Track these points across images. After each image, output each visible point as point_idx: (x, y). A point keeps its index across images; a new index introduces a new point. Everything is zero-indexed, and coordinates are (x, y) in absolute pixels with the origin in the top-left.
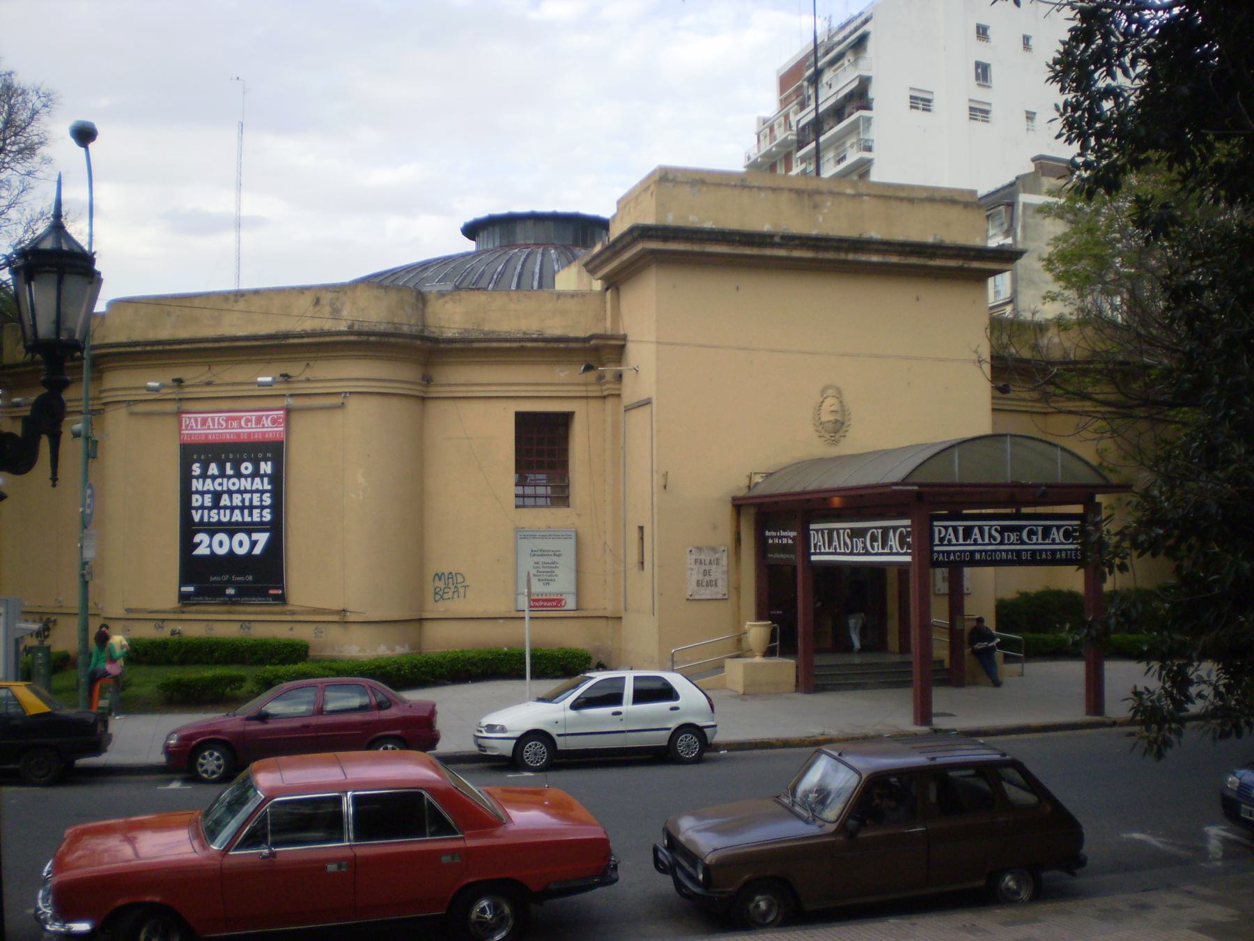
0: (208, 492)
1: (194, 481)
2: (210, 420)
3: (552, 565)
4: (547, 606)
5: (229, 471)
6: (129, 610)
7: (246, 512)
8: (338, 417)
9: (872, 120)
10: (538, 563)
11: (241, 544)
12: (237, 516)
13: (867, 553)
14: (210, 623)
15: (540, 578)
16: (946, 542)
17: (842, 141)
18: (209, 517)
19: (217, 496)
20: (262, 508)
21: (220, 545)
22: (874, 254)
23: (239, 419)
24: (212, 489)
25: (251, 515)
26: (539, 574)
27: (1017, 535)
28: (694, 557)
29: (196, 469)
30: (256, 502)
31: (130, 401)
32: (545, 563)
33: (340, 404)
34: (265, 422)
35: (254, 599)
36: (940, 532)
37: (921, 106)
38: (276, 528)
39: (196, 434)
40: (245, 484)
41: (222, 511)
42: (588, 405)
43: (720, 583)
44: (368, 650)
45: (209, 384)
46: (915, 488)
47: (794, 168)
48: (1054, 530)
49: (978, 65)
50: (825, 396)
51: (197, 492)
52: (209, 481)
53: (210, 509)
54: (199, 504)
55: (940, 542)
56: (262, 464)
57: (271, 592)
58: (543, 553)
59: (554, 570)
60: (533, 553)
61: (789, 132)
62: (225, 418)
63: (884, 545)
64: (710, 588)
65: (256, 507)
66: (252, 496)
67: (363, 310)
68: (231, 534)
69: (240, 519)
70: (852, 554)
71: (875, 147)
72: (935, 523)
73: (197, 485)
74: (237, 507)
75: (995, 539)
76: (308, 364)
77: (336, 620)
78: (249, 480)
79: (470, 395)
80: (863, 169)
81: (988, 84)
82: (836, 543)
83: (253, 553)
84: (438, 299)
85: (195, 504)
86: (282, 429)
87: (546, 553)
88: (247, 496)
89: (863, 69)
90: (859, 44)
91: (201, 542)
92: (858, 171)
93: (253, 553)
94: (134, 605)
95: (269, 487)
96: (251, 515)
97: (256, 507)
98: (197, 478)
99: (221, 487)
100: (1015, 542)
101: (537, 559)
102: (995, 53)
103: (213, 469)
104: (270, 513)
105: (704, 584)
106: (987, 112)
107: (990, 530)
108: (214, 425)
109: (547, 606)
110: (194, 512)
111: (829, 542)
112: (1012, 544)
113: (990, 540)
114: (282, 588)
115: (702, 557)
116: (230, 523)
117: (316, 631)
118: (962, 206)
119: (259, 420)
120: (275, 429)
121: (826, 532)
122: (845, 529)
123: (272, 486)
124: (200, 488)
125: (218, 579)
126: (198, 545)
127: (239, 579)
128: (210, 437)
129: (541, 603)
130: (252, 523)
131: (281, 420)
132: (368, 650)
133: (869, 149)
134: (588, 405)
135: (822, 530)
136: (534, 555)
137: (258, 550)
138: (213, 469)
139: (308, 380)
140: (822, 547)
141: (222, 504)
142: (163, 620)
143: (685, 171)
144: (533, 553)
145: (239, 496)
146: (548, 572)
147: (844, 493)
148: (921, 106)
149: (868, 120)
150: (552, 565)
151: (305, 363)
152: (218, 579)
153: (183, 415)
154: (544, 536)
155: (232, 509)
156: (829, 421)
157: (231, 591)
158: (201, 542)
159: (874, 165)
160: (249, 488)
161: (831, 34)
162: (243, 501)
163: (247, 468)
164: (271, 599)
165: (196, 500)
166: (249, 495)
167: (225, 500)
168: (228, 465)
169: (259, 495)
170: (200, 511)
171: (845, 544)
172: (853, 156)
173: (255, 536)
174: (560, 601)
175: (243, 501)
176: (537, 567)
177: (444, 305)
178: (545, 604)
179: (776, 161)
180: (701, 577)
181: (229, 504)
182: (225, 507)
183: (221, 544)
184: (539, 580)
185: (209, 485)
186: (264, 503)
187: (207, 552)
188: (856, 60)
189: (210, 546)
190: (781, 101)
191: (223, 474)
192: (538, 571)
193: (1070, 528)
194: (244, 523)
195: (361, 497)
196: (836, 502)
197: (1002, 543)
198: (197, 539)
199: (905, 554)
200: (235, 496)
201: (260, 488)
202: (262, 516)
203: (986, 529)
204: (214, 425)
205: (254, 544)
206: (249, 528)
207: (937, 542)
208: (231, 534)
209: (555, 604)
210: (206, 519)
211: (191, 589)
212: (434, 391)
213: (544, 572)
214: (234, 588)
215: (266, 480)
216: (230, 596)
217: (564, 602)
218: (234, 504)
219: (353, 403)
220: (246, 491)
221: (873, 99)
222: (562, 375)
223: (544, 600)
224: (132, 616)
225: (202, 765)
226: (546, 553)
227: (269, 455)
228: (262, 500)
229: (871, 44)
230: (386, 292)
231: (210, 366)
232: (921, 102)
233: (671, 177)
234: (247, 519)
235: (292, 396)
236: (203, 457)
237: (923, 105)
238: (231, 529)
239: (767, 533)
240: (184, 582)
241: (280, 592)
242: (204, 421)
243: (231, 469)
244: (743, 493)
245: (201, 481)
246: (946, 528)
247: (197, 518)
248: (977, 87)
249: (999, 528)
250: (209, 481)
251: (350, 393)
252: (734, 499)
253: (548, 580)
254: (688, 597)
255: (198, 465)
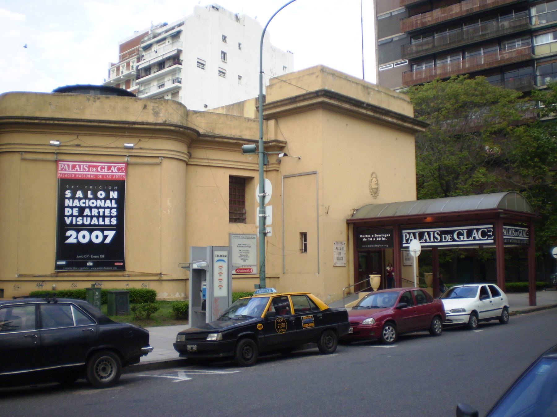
0: (76, 207)
1: (67, 201)
2: (77, 166)
3: (247, 252)
4: (245, 272)
5: (90, 195)
6: (20, 276)
7: (101, 219)
8: (157, 170)
9: (182, 69)
10: (241, 250)
11: (97, 237)
12: (95, 221)
13: (519, 237)
14: (75, 283)
15: (242, 258)
16: (64, 170)
17: (163, 77)
18: (77, 221)
19: (81, 210)
20: (111, 217)
21: (84, 237)
22: (391, 118)
23: (97, 167)
24: (78, 205)
25: (104, 221)
26: (241, 256)
27: (450, 236)
28: (336, 246)
29: (68, 194)
30: (107, 214)
31: (22, 152)
32: (244, 251)
33: (160, 163)
34: (476, 235)
35: (106, 268)
36: (61, 166)
37: (201, 67)
38: (119, 228)
39: (68, 174)
40: (100, 203)
41: (85, 218)
42: (267, 174)
43: (344, 259)
44: (172, 295)
45: (78, 146)
46: (503, 211)
47: (131, 86)
48: (475, 231)
49: (222, 52)
50: (373, 177)
51: (69, 207)
52: (76, 201)
53: (77, 217)
54: (70, 213)
55: (406, 241)
56: (111, 193)
57: (116, 264)
58: (243, 246)
59: (248, 254)
60: (239, 246)
61: (132, 71)
62: (87, 166)
63: (522, 234)
64: (340, 261)
65: (107, 217)
66: (105, 210)
67: (171, 114)
68: (91, 231)
69: (97, 223)
70: (515, 236)
71: (183, 81)
72: (404, 231)
73: (68, 202)
74: (95, 216)
75: (437, 239)
76: (140, 140)
77: (157, 279)
78: (103, 201)
79: (211, 165)
80: (175, 92)
81: (225, 61)
82: (510, 233)
83: (105, 242)
84: (193, 114)
85: (67, 213)
86: (124, 174)
87: (244, 246)
88: (101, 210)
89: (177, 46)
90: (176, 36)
91: (71, 235)
92: (172, 92)
93: (105, 242)
94: (23, 272)
95: (116, 206)
96: (104, 221)
97: (107, 217)
98: (69, 199)
99: (85, 204)
100: (449, 240)
101: (240, 249)
102: (230, 48)
103: (79, 194)
104: (116, 220)
105: (339, 259)
106: (224, 73)
107: (434, 234)
108: (80, 169)
109: (245, 272)
110: (66, 218)
111: (508, 232)
112: (447, 241)
113: (434, 240)
114: (124, 262)
115: (338, 246)
116: (90, 225)
117: (143, 286)
118: (407, 102)
119: (109, 168)
120: (119, 174)
121: (507, 229)
122: (513, 229)
123: (117, 205)
124: (71, 205)
125: (82, 257)
126: (69, 237)
127: (95, 257)
128: (77, 176)
129: (242, 271)
130: (105, 225)
131: (123, 169)
132: (172, 295)
133: (180, 82)
134: (267, 174)
135: (506, 228)
136: (239, 247)
137: (108, 241)
138: (79, 194)
139: (141, 149)
140: (506, 234)
141: (85, 214)
142: (43, 281)
143: (329, 69)
144: (239, 246)
145: (96, 210)
146: (245, 255)
147: (432, 216)
148: (201, 67)
149: (180, 70)
150: (247, 252)
151: (139, 139)
152: (82, 257)
153: (59, 162)
154: (244, 237)
155: (92, 217)
156: (375, 188)
157: (90, 264)
158: (71, 235)
159: (182, 90)
160: (102, 205)
161: (153, 29)
162: (99, 213)
163: (101, 194)
164: (116, 268)
165: (68, 212)
166: (103, 210)
167: (87, 212)
168: (89, 192)
169: (109, 210)
170: (70, 218)
171: (513, 233)
172: (169, 85)
173: (106, 233)
174: (250, 269)
175: (99, 213)
176: (240, 253)
177: (196, 118)
178: (244, 271)
179: (120, 83)
180: (338, 256)
181: (89, 214)
182: (87, 216)
183: (84, 237)
184: (241, 259)
185: (76, 203)
186: (112, 215)
187: (75, 241)
188: (173, 43)
189: (77, 238)
190: (120, 56)
191: (85, 197)
192: (241, 255)
193: (486, 230)
194: (99, 225)
195: (169, 213)
196: (429, 219)
197: (441, 241)
198: (68, 233)
199: (527, 237)
200: (93, 210)
201: (110, 206)
202: (111, 222)
203: (432, 233)
204: (80, 169)
205: (105, 237)
206: (103, 228)
207: (404, 242)
208: (91, 231)
209: (248, 271)
210: (74, 223)
211: (64, 263)
212: (193, 162)
213: (243, 255)
214: (92, 262)
215: (113, 202)
216: (90, 267)
217: (252, 270)
218: (93, 214)
219: (166, 162)
220: (101, 207)
221: (182, 61)
222: (250, 158)
223: (243, 269)
224: (22, 279)
225: (387, 338)
226: (244, 246)
227: (116, 188)
228: (111, 213)
229: (182, 36)
230: (180, 107)
231: (78, 136)
232: (201, 65)
233: (325, 70)
234: (101, 223)
235: (129, 156)
236: (73, 187)
237: (202, 66)
238: (91, 229)
239: (361, 236)
240: (59, 258)
241: (122, 264)
242: (74, 167)
243: (91, 195)
244: (349, 218)
245: (71, 200)
246: (409, 233)
247: (68, 221)
248: (222, 62)
249: (439, 232)
250: (76, 201)
251: (164, 157)
252: (348, 220)
253: (245, 259)
254: (334, 265)
255: (69, 191)
